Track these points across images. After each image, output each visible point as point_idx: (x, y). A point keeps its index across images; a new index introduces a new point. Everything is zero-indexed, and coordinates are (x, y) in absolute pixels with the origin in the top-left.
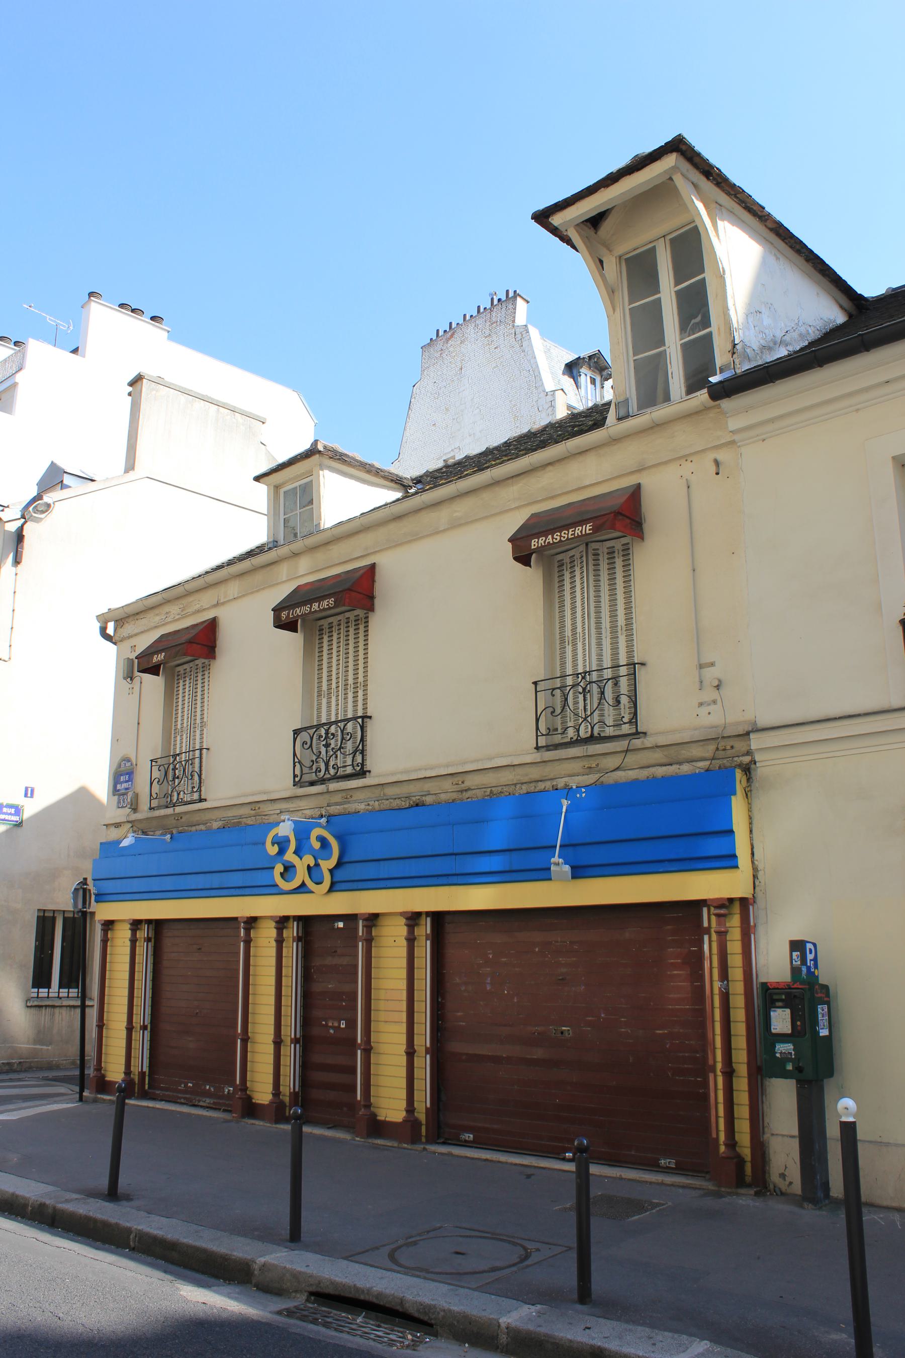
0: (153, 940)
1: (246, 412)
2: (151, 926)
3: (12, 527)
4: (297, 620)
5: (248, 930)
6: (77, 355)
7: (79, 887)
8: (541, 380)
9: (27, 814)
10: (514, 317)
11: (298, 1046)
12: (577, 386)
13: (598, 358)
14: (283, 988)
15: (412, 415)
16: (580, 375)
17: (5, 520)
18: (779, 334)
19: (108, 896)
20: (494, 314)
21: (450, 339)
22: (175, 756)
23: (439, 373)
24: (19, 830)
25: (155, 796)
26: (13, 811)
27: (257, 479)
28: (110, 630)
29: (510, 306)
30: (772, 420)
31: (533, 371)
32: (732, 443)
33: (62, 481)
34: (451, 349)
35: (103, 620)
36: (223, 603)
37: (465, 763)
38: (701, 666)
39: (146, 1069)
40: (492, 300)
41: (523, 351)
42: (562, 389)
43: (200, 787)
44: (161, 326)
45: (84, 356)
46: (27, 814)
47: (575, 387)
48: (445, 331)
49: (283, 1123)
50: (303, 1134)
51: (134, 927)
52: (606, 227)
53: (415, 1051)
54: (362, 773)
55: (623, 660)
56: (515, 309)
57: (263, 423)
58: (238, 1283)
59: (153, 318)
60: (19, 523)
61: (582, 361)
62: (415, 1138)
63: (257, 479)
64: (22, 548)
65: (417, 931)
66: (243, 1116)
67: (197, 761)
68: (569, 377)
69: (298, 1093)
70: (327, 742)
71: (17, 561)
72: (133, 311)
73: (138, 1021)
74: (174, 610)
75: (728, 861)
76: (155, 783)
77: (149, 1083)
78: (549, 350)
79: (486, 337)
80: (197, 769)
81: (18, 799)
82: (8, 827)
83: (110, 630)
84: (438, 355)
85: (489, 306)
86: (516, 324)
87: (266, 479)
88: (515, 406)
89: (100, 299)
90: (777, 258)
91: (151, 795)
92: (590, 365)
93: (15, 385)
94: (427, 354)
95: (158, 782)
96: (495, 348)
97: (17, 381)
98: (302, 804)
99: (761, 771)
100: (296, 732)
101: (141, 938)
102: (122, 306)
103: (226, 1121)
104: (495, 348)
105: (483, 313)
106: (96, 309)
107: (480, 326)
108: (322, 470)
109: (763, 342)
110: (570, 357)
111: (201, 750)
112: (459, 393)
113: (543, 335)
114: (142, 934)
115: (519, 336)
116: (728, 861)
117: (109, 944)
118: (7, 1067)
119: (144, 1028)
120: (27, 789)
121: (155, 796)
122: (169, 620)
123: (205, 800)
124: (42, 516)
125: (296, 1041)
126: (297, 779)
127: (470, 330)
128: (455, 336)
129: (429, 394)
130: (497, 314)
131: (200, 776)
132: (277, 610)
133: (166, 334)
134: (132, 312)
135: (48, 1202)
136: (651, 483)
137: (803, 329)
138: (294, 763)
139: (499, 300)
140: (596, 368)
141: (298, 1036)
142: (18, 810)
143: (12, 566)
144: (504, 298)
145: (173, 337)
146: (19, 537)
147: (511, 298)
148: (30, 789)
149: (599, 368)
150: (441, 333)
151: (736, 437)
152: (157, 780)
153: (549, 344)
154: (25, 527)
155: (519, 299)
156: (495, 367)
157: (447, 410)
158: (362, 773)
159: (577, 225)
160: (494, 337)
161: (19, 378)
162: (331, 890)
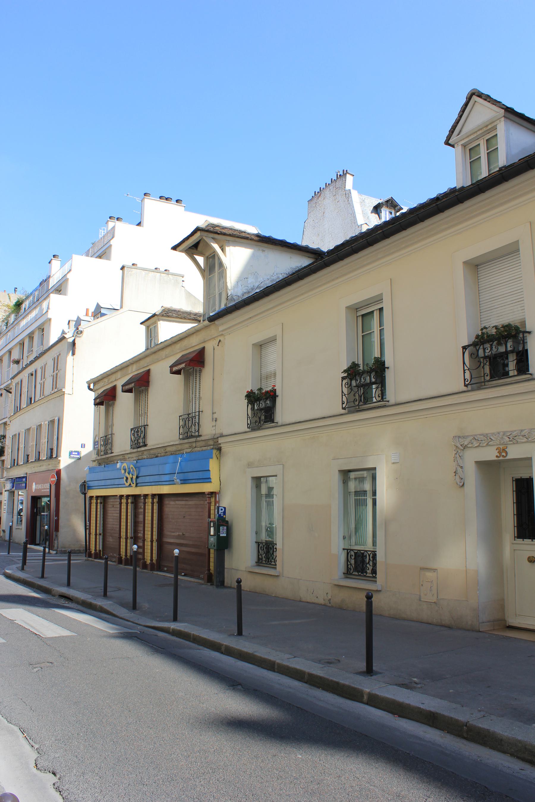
0: (103, 503)
1: (174, 273)
2: (102, 498)
3: (70, 340)
4: (133, 389)
5: (145, 499)
6: (140, 226)
7: (82, 484)
8: (356, 219)
9: (82, 454)
10: (345, 185)
11: (132, 540)
12: (379, 218)
13: (392, 201)
14: (146, 521)
15: (304, 238)
16: (381, 212)
17: (67, 338)
18: (256, 285)
19: (189, 481)
20: (337, 183)
21: (319, 197)
22: (189, 414)
23: (315, 215)
24: (80, 461)
25: (181, 433)
26: (77, 453)
27: (141, 323)
28: (92, 387)
29: (344, 179)
30: (229, 328)
31: (353, 214)
32: (222, 335)
33: (100, 312)
34: (320, 202)
35: (89, 383)
36: (117, 380)
37: (170, 442)
38: (213, 414)
39: (101, 549)
40: (337, 175)
41: (349, 204)
42: (366, 223)
43: (198, 430)
44: (181, 205)
45: (143, 227)
46: (82, 454)
47: (378, 219)
48: (318, 192)
49: (145, 569)
50: (22, 550)
51: (145, 498)
52: (200, 247)
53: (121, 537)
54: (145, 445)
55: (197, 410)
56: (346, 181)
57: (183, 277)
58: (448, 732)
59: (177, 201)
60: (73, 338)
61: (381, 204)
62: (152, 569)
63: (141, 323)
64: (75, 348)
65: (147, 500)
66: (119, 564)
67: (197, 417)
68: (375, 214)
69: (132, 556)
70: (492, 352)
71: (73, 354)
72: (167, 199)
73: (129, 535)
74: (134, 367)
75: (208, 480)
76: (181, 428)
77: (102, 554)
78: (364, 201)
79: (334, 196)
80: (197, 421)
81: (79, 449)
82: (75, 460)
83: (92, 387)
84: (314, 205)
85: (336, 179)
86: (346, 189)
87: (144, 324)
88: (346, 233)
89: (149, 197)
90: (263, 251)
91: (180, 433)
92: (388, 205)
93: (111, 246)
94: (310, 205)
95: (182, 427)
96: (338, 202)
97: (111, 244)
98: (134, 455)
99: (223, 450)
100: (464, 348)
101: (124, 502)
102: (161, 197)
103: (114, 565)
104: (338, 202)
105: (328, 186)
106: (148, 202)
107: (331, 190)
108: (159, 321)
109: (245, 291)
110: (376, 202)
111: (199, 412)
112: (323, 226)
113: (360, 192)
114: (156, 500)
115: (347, 195)
116: (208, 480)
117: (92, 504)
118: (78, 551)
119: (100, 534)
120: (82, 444)
121: (181, 433)
122: (105, 384)
123: (113, 453)
124: (81, 335)
125: (131, 538)
126: (344, 406)
127: (327, 192)
128: (321, 195)
129: (311, 227)
130: (339, 183)
131: (199, 424)
132: (171, 367)
133: (184, 208)
134: (166, 200)
135: (25, 578)
136: (209, 348)
137: (275, 278)
138: (464, 370)
139: (340, 175)
140: (392, 206)
141: (132, 536)
142: (79, 453)
143: (72, 356)
144: (342, 174)
145: (187, 209)
146: (74, 343)
147: (345, 174)
148: (83, 445)
149: (394, 206)
150: (317, 193)
151: (223, 333)
152: (182, 426)
153: (364, 197)
154: (76, 339)
155: (347, 175)
156: (337, 212)
157: (318, 235)
158: (145, 445)
159: (185, 251)
160: (337, 195)
161: (112, 242)
162: (136, 486)
